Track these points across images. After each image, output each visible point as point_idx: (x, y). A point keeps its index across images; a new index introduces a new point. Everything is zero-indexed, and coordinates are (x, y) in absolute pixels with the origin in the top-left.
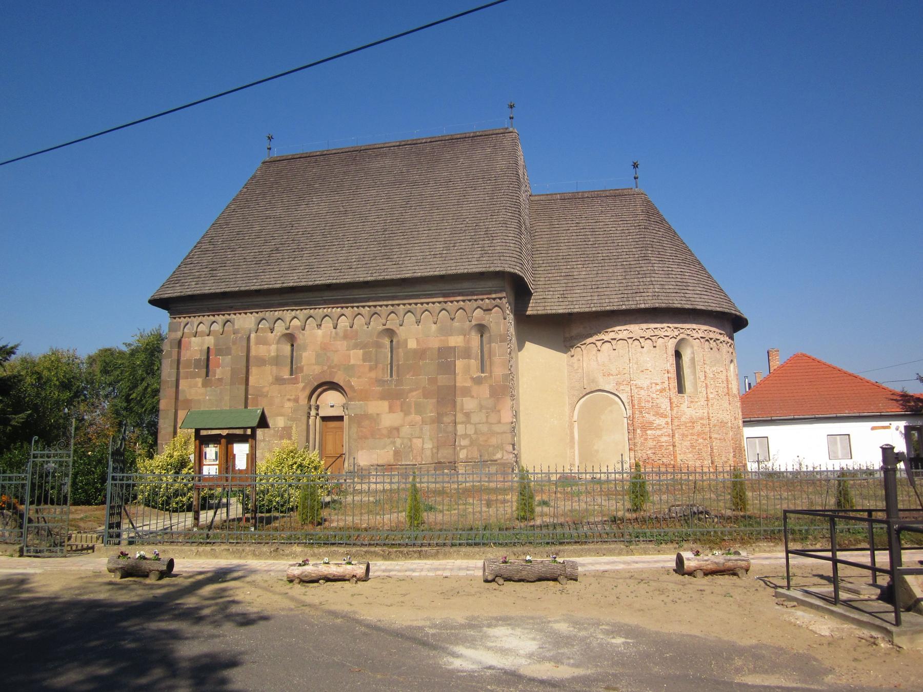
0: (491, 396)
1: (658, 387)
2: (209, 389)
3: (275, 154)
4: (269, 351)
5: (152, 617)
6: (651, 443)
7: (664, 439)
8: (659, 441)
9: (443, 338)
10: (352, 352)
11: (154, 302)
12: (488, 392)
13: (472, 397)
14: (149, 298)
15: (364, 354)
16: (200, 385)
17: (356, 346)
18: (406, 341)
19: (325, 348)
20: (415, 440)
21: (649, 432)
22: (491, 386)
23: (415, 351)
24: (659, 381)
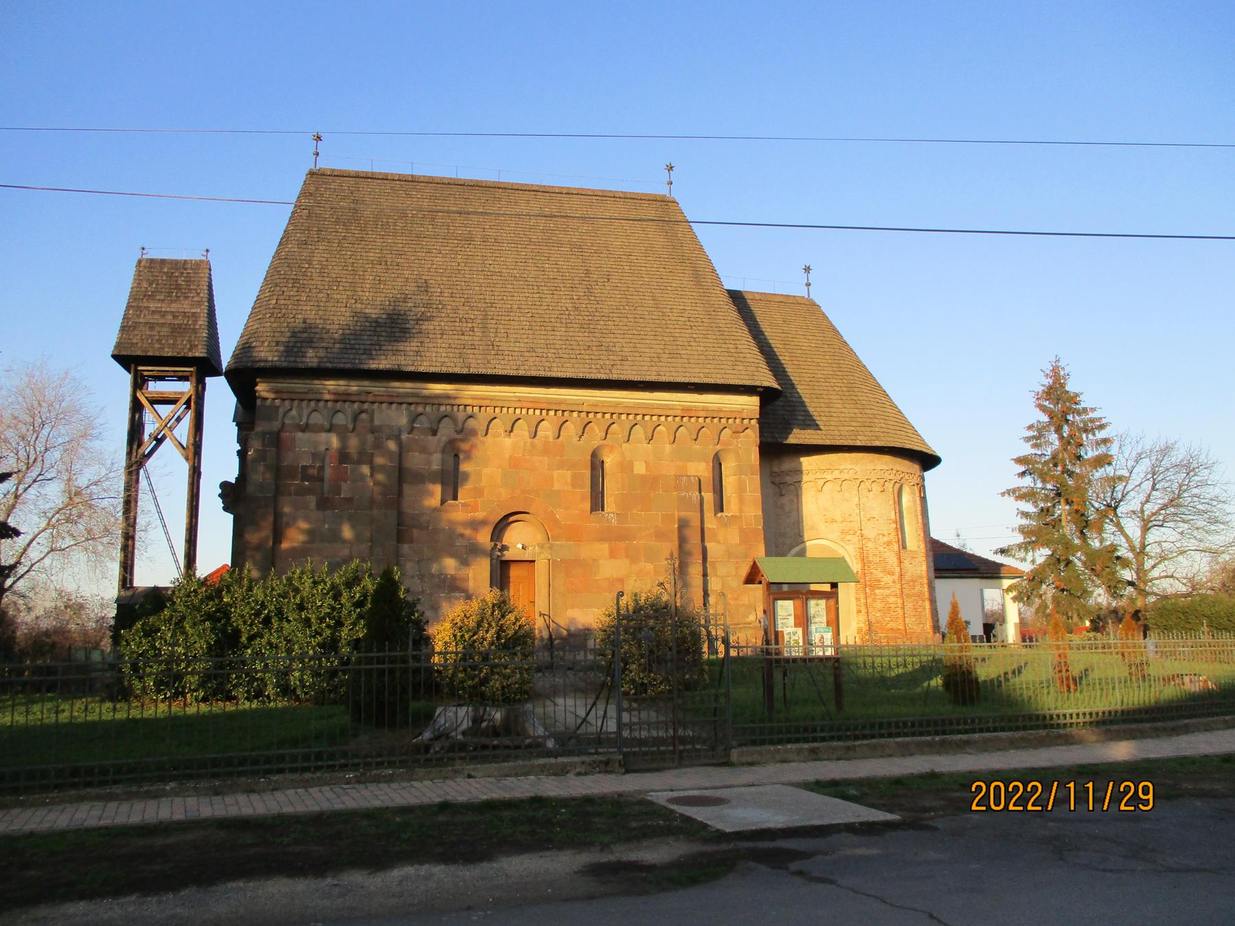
1: (885, 539)
2: (328, 513)
4: (429, 463)
5: (677, 865)
6: (879, 605)
7: (892, 599)
8: (888, 603)
9: (680, 463)
10: (556, 473)
13: (719, 542)
15: (574, 476)
16: (313, 505)
17: (561, 466)
19: (515, 463)
21: (877, 591)
22: (741, 531)
23: (643, 478)
24: (885, 533)
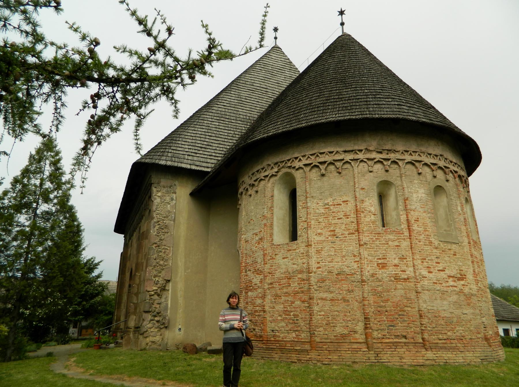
21: (250, 294)
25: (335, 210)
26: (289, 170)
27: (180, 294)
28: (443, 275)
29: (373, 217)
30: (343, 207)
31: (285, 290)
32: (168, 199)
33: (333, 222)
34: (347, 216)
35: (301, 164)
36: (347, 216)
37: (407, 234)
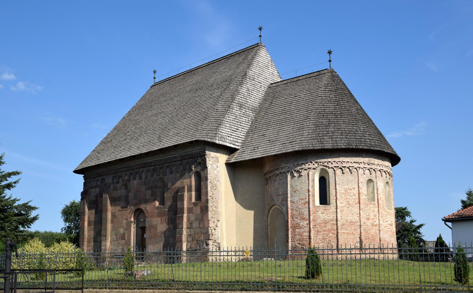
0: (201, 212)
3: (157, 80)
11: (76, 172)
12: (199, 210)
13: (193, 213)
14: (74, 170)
15: (152, 192)
18: (167, 184)
20: (170, 239)
21: (297, 230)
25: (349, 192)
26: (325, 168)
27: (224, 229)
28: (387, 223)
29: (365, 197)
30: (353, 191)
31: (323, 229)
32: (215, 166)
33: (348, 197)
34: (354, 195)
35: (333, 166)
36: (354, 195)
37: (377, 205)
